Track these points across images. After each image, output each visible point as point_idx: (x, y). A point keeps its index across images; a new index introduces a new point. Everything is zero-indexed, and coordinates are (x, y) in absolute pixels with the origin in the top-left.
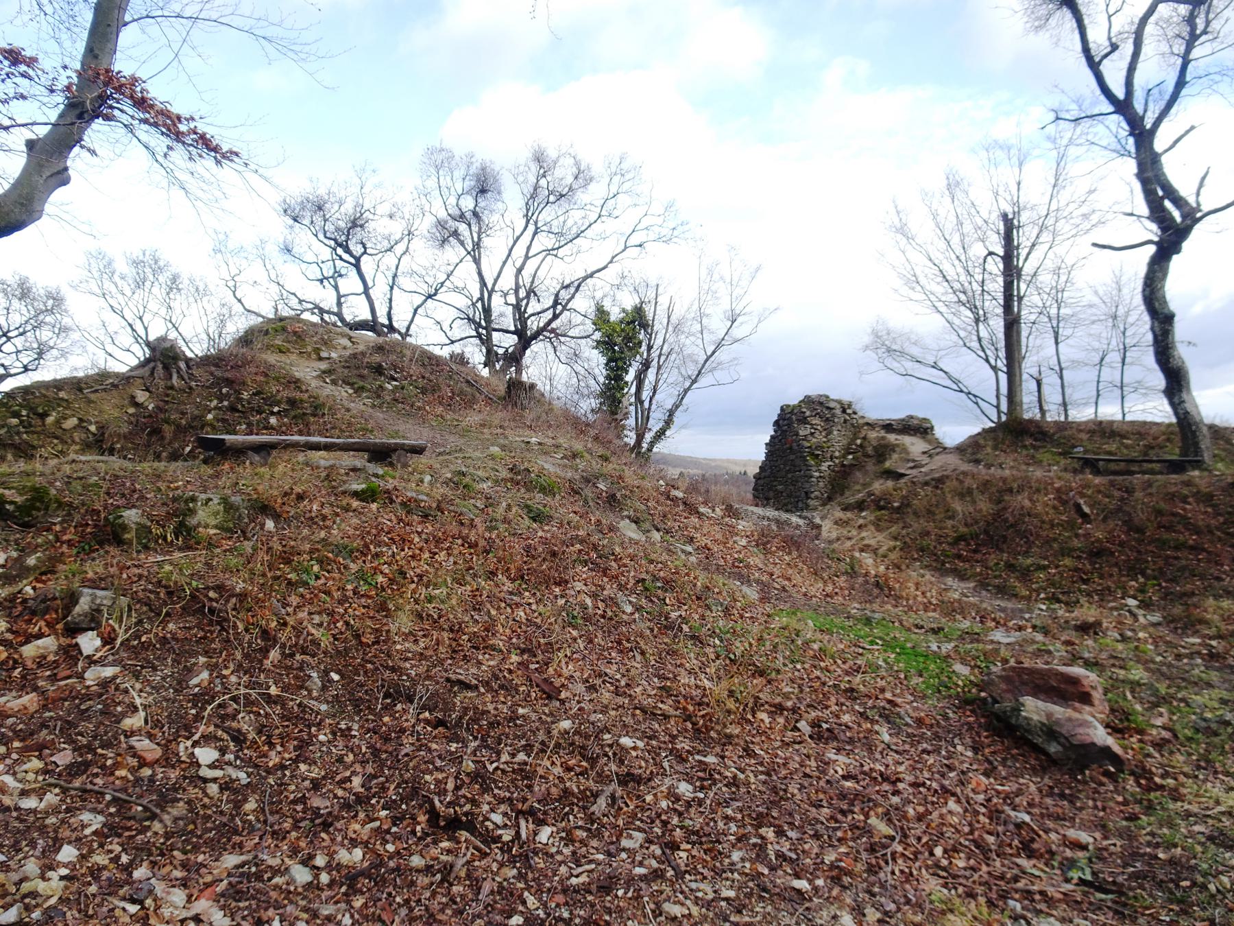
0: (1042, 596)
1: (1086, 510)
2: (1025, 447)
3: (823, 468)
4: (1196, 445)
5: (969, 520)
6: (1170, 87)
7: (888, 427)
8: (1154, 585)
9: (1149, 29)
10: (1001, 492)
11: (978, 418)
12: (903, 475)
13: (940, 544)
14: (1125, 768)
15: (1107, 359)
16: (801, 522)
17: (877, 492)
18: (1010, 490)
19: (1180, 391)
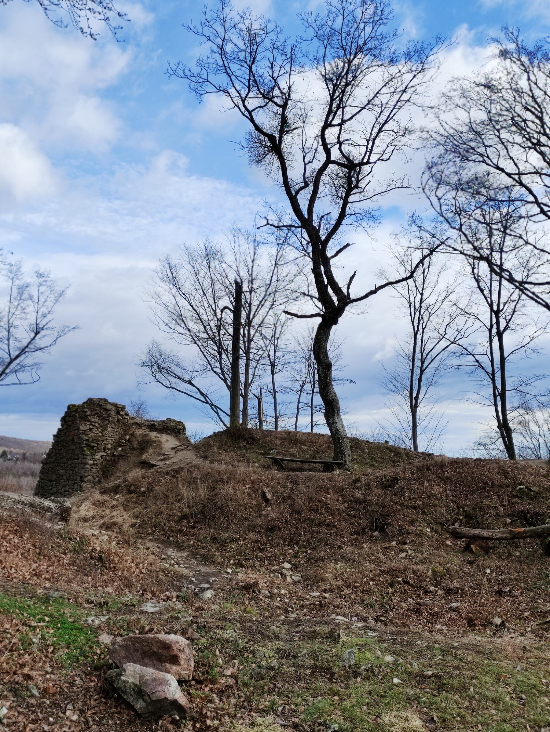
0: (232, 562)
1: (269, 496)
2: (240, 448)
3: (97, 457)
4: (342, 452)
6: (335, 215)
7: (152, 426)
8: (303, 552)
9: (324, 178)
10: (215, 481)
13: (169, 521)
14: (187, 715)
15: (305, 388)
16: (53, 505)
18: (222, 480)
19: (334, 415)
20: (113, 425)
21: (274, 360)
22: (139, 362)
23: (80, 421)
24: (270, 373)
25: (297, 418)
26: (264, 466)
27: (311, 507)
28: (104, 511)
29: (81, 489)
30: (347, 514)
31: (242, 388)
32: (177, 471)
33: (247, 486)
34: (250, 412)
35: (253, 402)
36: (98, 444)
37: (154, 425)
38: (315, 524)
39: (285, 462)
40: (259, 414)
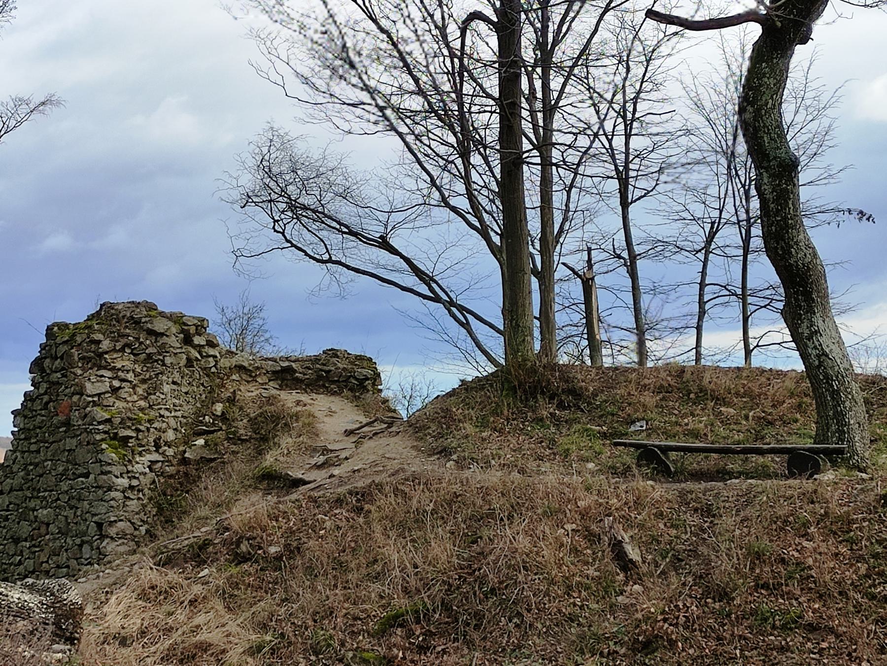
1: (633, 553)
4: (840, 417)
5: (413, 582)
7: (286, 375)
10: (474, 521)
11: (466, 356)
12: (298, 483)
15: (718, 240)
16: (32, 600)
17: (235, 526)
18: (491, 515)
20: (177, 377)
21: (627, 162)
22: (236, 195)
23: (85, 370)
24: (616, 201)
25: (699, 329)
26: (613, 471)
27: (758, 578)
28: (170, 614)
29: (101, 557)
30: (866, 595)
31: (534, 250)
32: (364, 496)
33: (569, 527)
34: (560, 318)
35: (569, 290)
36: (138, 431)
37: (289, 370)
38: (774, 627)
39: (673, 455)
40: (589, 325)
